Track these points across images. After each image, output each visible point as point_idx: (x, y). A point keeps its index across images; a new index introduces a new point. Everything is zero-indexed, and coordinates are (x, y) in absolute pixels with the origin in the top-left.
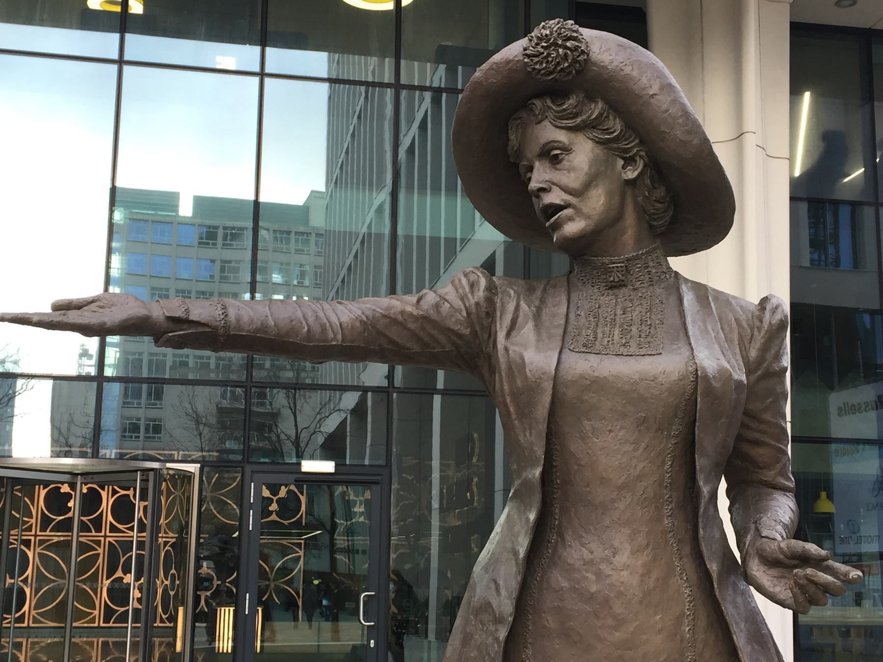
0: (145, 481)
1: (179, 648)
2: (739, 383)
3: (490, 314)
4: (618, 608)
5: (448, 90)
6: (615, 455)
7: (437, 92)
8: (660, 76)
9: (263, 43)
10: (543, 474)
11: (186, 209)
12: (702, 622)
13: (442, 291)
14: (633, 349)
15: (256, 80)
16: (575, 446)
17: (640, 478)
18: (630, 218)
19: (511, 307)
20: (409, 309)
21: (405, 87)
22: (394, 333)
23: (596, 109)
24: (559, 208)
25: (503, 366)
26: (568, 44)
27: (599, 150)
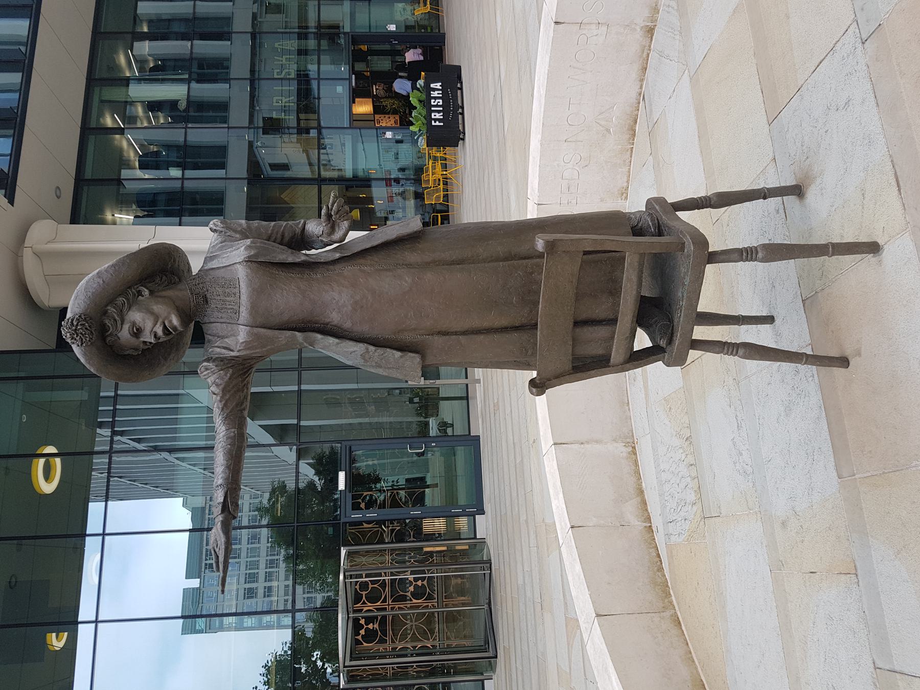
0: (351, 577)
1: (444, 548)
2: (252, 242)
3: (222, 360)
4: (358, 298)
5: (113, 427)
6: (289, 298)
7: (114, 433)
8: (93, 278)
9: (84, 535)
10: (299, 331)
11: (195, 583)
12: (362, 261)
13: (210, 383)
14: (237, 290)
15: (107, 538)
16: (285, 317)
17: (299, 288)
18: (170, 293)
19: (218, 350)
20: (219, 398)
21: (111, 447)
22: (231, 405)
23: (111, 309)
24: (165, 327)
25: (248, 352)
26: (75, 323)
27: (134, 308)
